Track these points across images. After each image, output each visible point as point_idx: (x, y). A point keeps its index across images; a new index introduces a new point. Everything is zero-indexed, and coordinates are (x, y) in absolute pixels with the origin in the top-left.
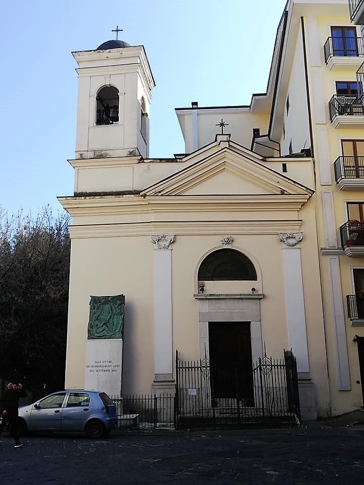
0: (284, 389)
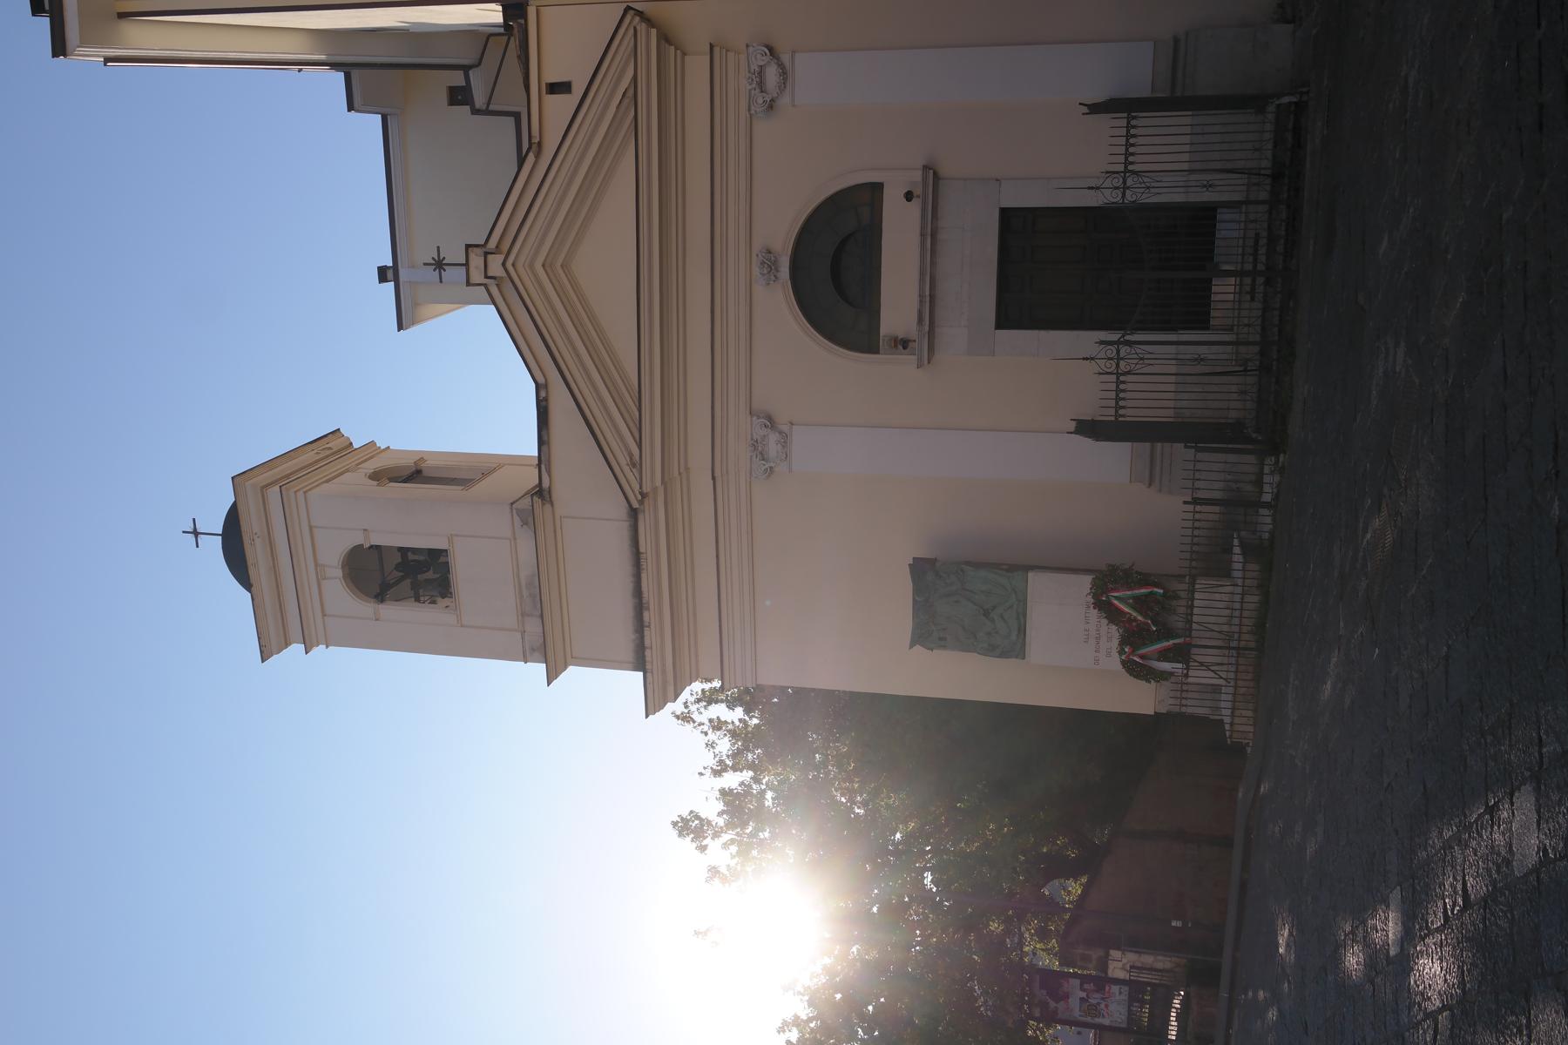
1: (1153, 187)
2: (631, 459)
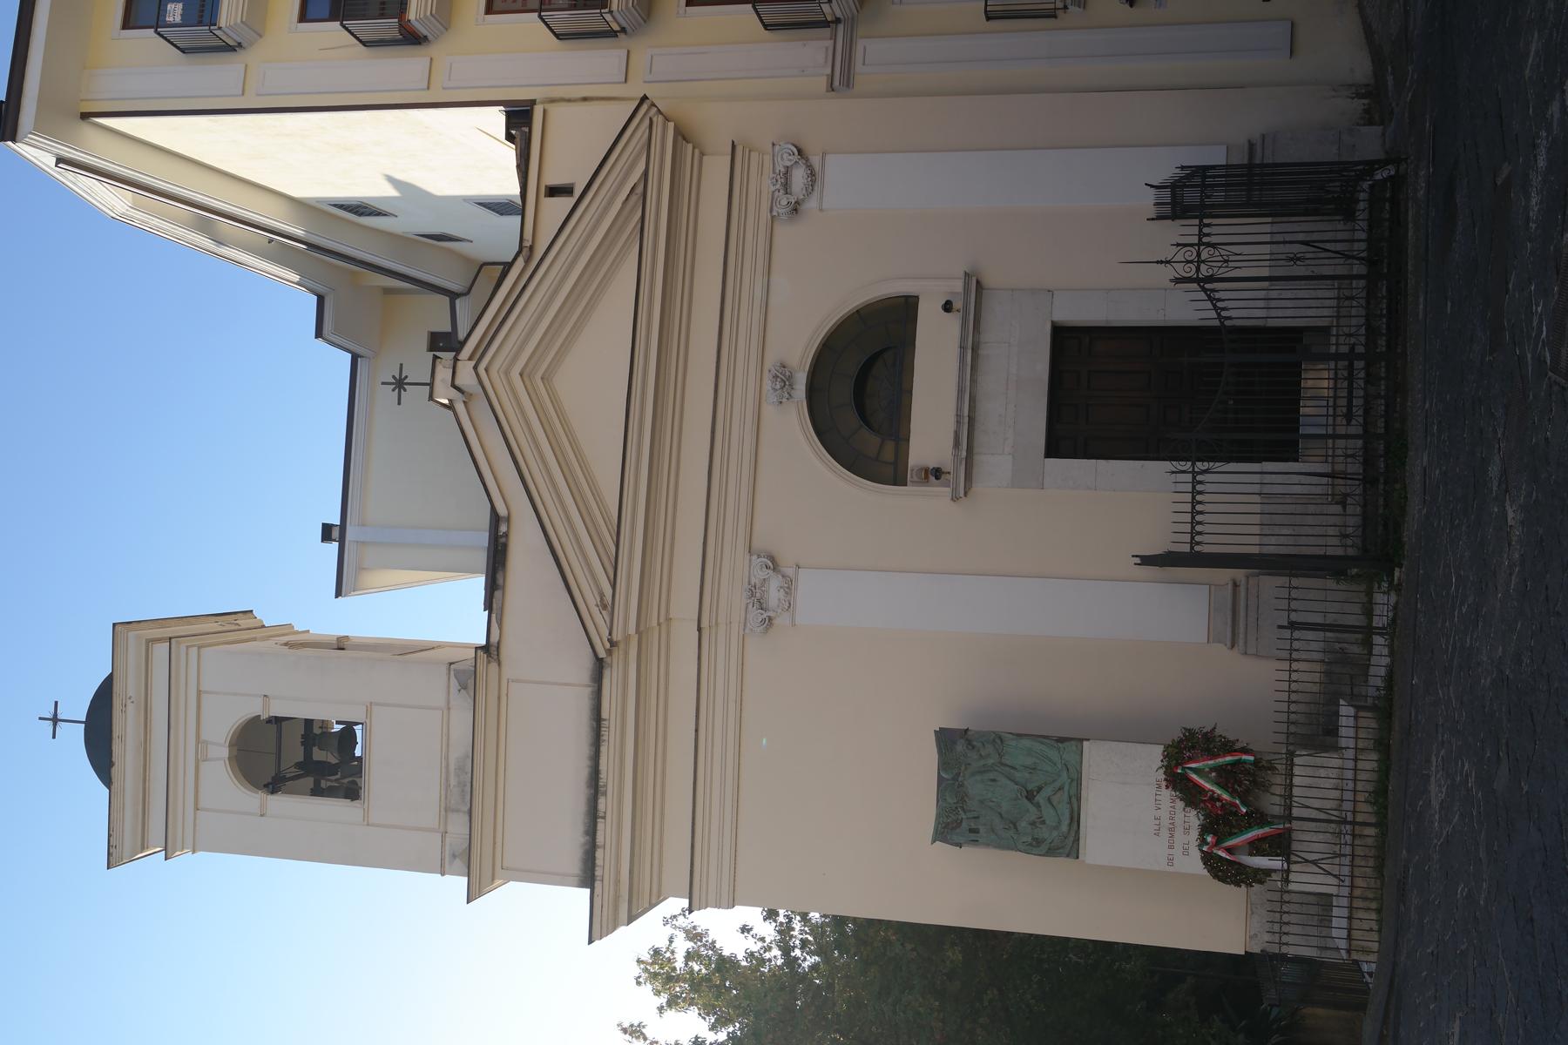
0: (1276, 228)
1: (1231, 261)
2: (602, 599)
